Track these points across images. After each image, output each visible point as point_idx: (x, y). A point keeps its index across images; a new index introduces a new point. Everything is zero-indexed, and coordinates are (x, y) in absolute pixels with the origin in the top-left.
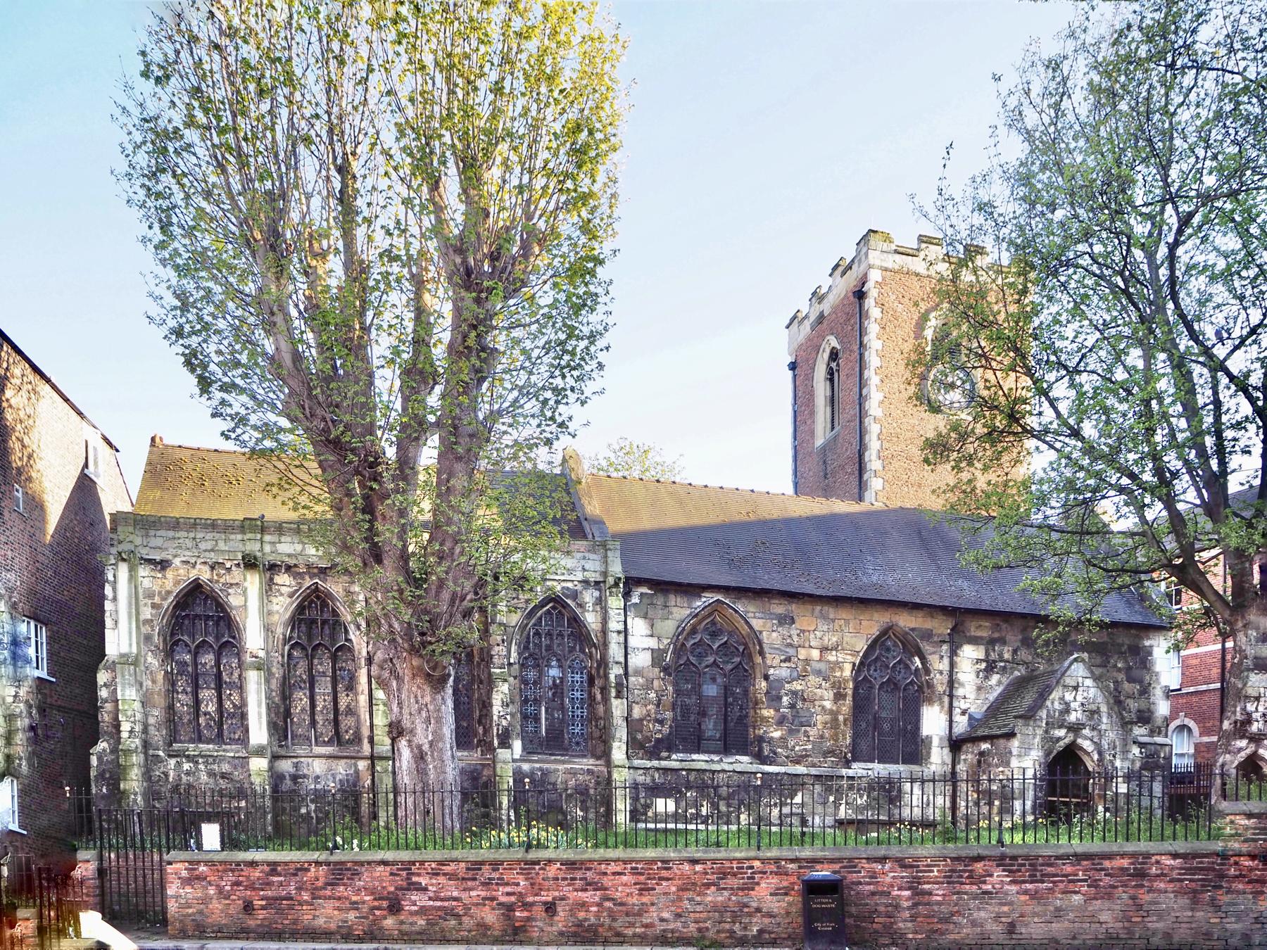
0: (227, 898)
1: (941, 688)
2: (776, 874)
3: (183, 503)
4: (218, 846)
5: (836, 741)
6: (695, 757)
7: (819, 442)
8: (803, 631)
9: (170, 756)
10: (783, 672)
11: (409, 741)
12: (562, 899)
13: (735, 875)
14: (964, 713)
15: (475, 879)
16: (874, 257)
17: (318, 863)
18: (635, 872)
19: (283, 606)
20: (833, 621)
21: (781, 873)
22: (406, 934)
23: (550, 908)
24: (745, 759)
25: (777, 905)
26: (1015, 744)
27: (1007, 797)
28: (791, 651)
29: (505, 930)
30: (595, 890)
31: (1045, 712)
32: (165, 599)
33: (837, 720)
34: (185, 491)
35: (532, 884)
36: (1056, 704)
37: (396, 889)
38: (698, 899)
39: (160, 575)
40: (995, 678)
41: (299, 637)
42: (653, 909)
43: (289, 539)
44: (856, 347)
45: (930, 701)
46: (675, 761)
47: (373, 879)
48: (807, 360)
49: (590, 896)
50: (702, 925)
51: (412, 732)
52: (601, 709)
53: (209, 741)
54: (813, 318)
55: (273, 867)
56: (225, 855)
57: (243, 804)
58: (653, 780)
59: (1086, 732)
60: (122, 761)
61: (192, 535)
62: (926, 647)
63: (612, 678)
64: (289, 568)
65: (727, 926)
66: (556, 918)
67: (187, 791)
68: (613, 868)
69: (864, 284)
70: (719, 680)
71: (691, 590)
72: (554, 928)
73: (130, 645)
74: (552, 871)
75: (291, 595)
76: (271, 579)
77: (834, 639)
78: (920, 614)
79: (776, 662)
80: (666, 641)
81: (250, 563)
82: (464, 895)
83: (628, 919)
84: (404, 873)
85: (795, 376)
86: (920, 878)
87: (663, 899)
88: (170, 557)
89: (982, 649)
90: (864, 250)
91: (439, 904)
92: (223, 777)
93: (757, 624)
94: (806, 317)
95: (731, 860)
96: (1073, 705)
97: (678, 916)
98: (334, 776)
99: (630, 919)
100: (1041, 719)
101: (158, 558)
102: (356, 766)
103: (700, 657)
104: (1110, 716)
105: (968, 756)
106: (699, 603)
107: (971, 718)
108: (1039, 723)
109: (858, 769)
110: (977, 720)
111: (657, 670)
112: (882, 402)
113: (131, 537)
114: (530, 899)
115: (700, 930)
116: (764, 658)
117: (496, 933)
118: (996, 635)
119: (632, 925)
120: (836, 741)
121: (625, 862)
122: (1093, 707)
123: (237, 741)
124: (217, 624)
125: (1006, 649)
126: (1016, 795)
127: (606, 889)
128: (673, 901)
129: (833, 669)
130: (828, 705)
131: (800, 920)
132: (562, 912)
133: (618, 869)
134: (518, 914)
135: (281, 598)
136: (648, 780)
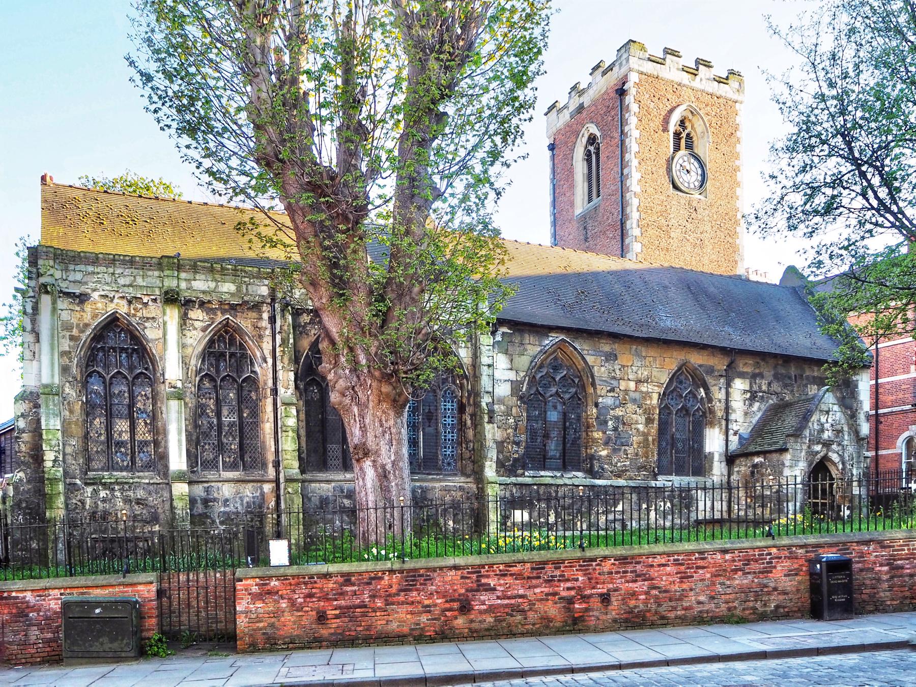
0: (300, 609)
1: (720, 414)
2: (789, 558)
3: (86, 240)
4: (286, 562)
5: (647, 457)
6: (542, 473)
7: (579, 210)
8: (623, 366)
9: (87, 484)
10: (609, 401)
11: (374, 461)
12: (616, 590)
13: (756, 561)
14: (735, 433)
15: (539, 577)
16: (634, 63)
17: (392, 571)
18: (677, 563)
19: (197, 339)
20: (645, 358)
21: (792, 557)
22: (476, 631)
23: (605, 599)
24: (580, 474)
25: (789, 584)
26: (787, 457)
27: (780, 500)
28: (615, 383)
29: (566, 622)
30: (644, 580)
31: (808, 431)
32: (83, 332)
33: (647, 440)
34: (87, 227)
35: (589, 579)
36: (815, 424)
37: (467, 590)
38: (728, 582)
39: (78, 308)
40: (756, 405)
41: (209, 369)
42: (692, 593)
43: (203, 277)
44: (617, 135)
45: (712, 424)
46: (527, 478)
47: (445, 583)
48: (566, 143)
49: (640, 586)
50: (730, 604)
51: (377, 453)
52: (470, 433)
53: (121, 469)
54: (572, 107)
55: (347, 578)
56: (294, 570)
57: (157, 528)
58: (512, 495)
59: (834, 447)
60: (47, 490)
61: (111, 270)
62: (710, 380)
63: (484, 405)
64: (202, 304)
65: (751, 604)
66: (610, 607)
67: (104, 518)
68: (659, 560)
69: (624, 84)
70: (559, 407)
71: (541, 330)
72: (609, 616)
73: (53, 376)
74: (607, 566)
75: (204, 330)
76: (186, 314)
77: (646, 373)
78: (705, 353)
79: (604, 392)
80: (522, 374)
81: (171, 298)
82: (529, 593)
83: (670, 604)
84: (474, 576)
85: (554, 155)
86: (894, 555)
87: (700, 585)
88: (89, 291)
89: (748, 381)
90: (625, 56)
91: (506, 602)
92: (138, 503)
93: (590, 359)
94: (565, 107)
95: (753, 549)
96: (826, 425)
97: (712, 598)
98: (241, 499)
99: (673, 604)
100: (806, 437)
101: (77, 291)
102: (261, 489)
103: (546, 387)
104: (849, 434)
105: (742, 468)
106: (547, 342)
107: (741, 437)
108: (804, 440)
109: (662, 481)
110: (745, 439)
111: (515, 398)
112: (640, 181)
113: (52, 271)
114: (588, 592)
115: (729, 609)
116: (595, 389)
117: (558, 624)
118: (757, 371)
119: (674, 609)
120: (647, 457)
121: (669, 555)
122: (839, 427)
123: (148, 467)
124: (129, 356)
125: (764, 382)
126: (790, 498)
127: (653, 579)
128: (707, 586)
129: (644, 398)
130: (641, 427)
131: (807, 595)
132: (615, 602)
133: (663, 561)
134: (577, 606)
135: (195, 332)
136: (508, 494)
